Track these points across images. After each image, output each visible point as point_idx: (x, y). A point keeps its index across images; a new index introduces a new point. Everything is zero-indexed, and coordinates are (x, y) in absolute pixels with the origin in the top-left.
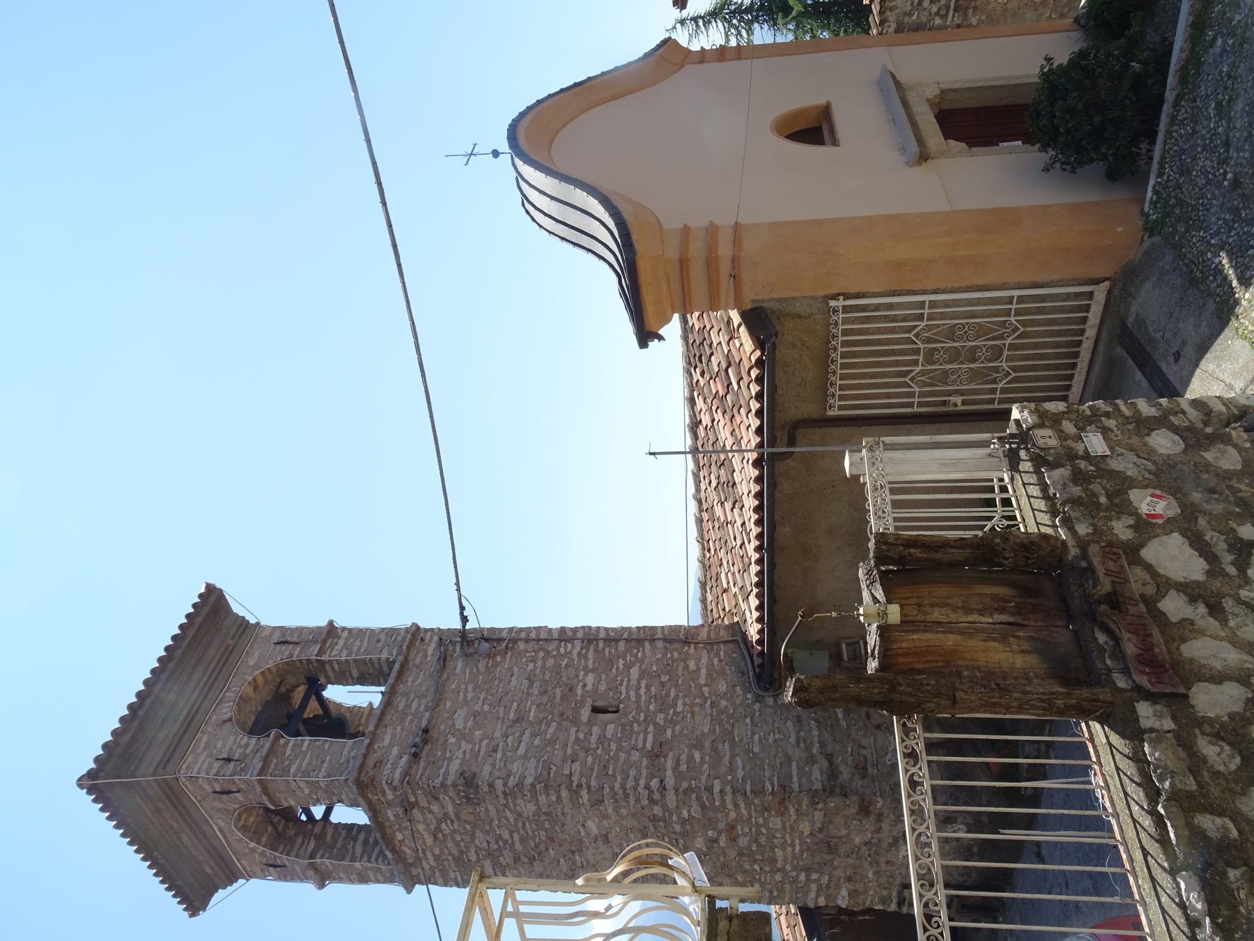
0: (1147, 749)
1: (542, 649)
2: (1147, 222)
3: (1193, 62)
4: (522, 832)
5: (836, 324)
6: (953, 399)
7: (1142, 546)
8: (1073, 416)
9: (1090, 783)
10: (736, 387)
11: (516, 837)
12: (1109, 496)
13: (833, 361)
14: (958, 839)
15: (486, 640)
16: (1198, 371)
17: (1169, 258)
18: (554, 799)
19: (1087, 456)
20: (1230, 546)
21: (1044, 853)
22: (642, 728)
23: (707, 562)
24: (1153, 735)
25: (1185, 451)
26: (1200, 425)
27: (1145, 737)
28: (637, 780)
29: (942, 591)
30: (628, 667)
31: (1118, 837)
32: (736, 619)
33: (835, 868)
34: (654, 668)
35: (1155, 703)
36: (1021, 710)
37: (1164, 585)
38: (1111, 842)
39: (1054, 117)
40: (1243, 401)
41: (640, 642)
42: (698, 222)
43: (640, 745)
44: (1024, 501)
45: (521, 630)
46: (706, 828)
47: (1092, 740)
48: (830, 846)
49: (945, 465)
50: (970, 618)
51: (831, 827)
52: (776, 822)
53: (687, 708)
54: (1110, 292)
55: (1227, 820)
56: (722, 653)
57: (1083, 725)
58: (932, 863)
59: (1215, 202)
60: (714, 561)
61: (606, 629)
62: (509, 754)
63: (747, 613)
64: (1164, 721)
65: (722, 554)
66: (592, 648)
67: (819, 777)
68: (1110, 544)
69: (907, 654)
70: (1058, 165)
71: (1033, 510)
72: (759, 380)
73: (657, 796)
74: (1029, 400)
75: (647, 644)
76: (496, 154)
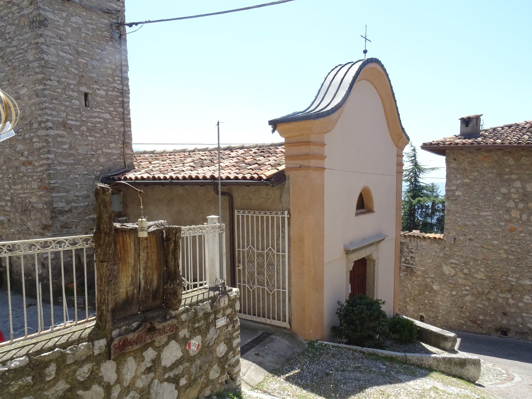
0: (84, 343)
1: (117, 67)
2: (314, 342)
3: (377, 358)
4: (17, 52)
5: (277, 214)
6: (241, 265)
7: (176, 341)
8: (233, 313)
9: (67, 320)
10: (249, 168)
11: (14, 49)
12: (198, 327)
13: (260, 212)
14: (35, 270)
15: (120, 37)
16: (251, 363)
17: (298, 350)
18: (37, 70)
19: (216, 318)
20: (177, 375)
21: (31, 307)
22: (78, 119)
23: (164, 154)
24: (91, 346)
25: (217, 357)
26: (228, 363)
27: (90, 343)
28: (51, 115)
29: (154, 257)
30: (110, 113)
31: (42, 332)
32: (136, 168)
33: (14, 214)
34: (110, 126)
35: (106, 347)
36: (100, 291)
37: (159, 350)
38: (39, 330)
39: (360, 305)
40: (238, 379)
41: (123, 119)
42: (327, 151)
43: (69, 118)
44: (196, 293)
45: (126, 57)
46: (28, 150)
47: (87, 321)
48: (25, 211)
49: (213, 265)
50: (142, 270)
51: (35, 212)
52: (35, 185)
53: (90, 142)
54: (286, 328)
55: (54, 376)
56: (119, 160)
57: (94, 318)
58: (21, 251)
59: (320, 367)
60: (165, 158)
61: (128, 102)
62: (59, 47)
63: (140, 173)
64: (98, 350)
65: (168, 161)
66: (119, 94)
67: (60, 206)
68: (177, 328)
69: (123, 241)
70: (340, 307)
71: (192, 297)
72: (252, 178)
73: (43, 125)
74: (240, 295)
75: (122, 123)
76: (365, 52)
